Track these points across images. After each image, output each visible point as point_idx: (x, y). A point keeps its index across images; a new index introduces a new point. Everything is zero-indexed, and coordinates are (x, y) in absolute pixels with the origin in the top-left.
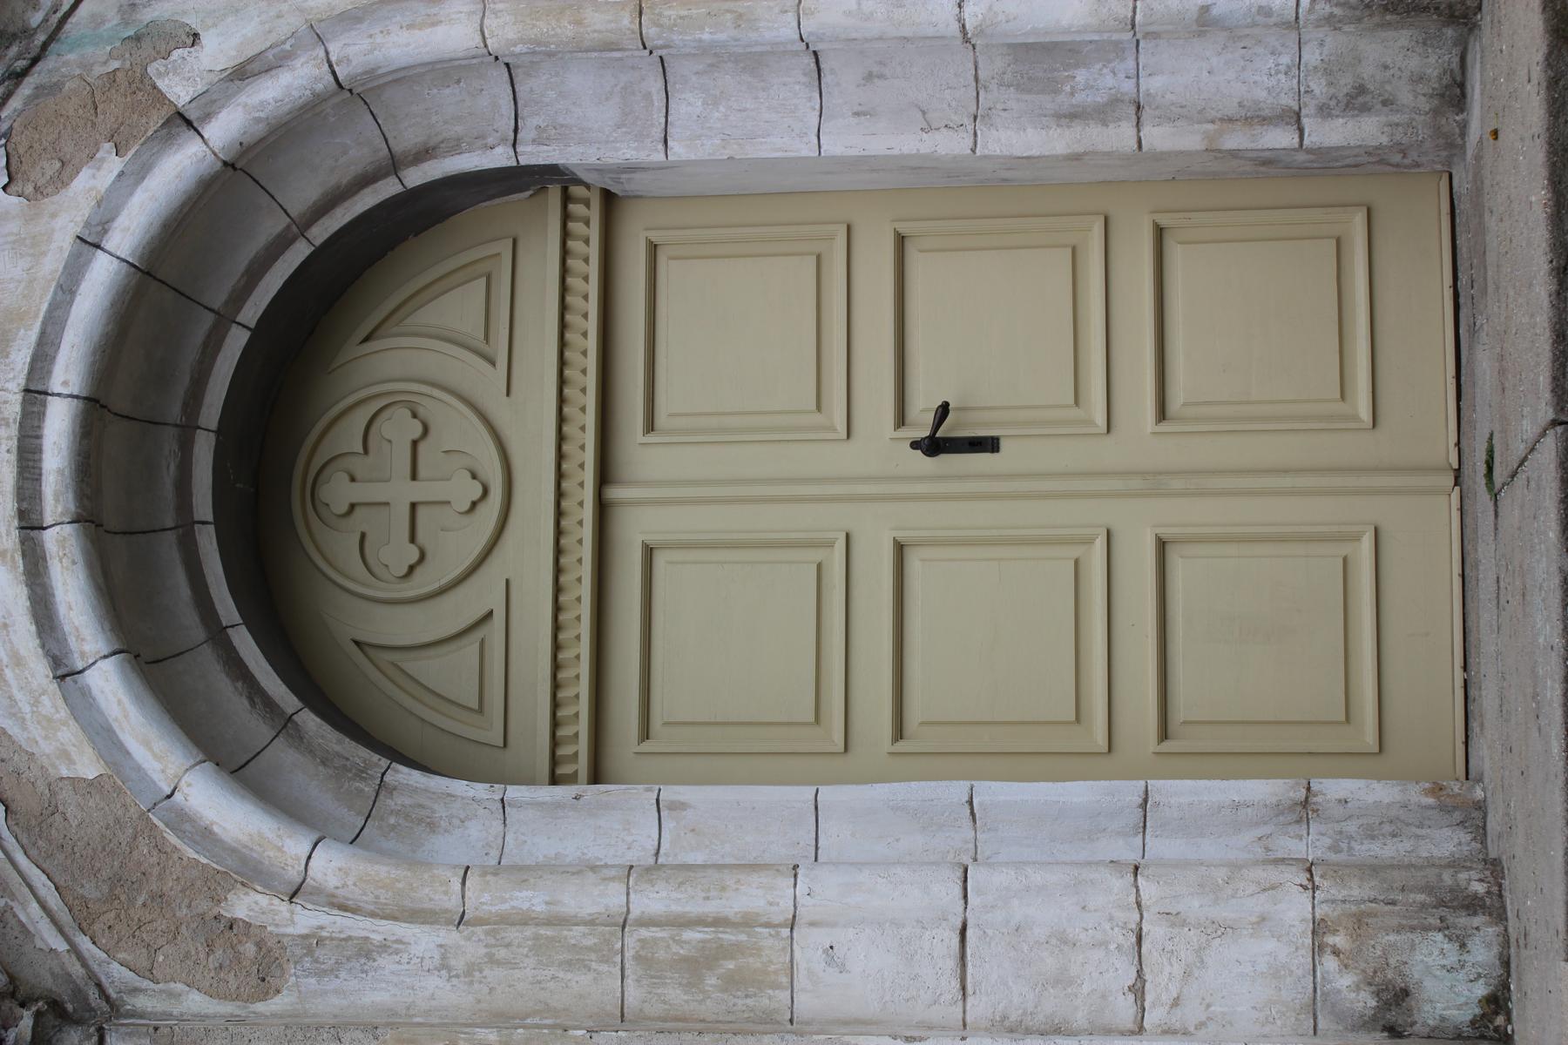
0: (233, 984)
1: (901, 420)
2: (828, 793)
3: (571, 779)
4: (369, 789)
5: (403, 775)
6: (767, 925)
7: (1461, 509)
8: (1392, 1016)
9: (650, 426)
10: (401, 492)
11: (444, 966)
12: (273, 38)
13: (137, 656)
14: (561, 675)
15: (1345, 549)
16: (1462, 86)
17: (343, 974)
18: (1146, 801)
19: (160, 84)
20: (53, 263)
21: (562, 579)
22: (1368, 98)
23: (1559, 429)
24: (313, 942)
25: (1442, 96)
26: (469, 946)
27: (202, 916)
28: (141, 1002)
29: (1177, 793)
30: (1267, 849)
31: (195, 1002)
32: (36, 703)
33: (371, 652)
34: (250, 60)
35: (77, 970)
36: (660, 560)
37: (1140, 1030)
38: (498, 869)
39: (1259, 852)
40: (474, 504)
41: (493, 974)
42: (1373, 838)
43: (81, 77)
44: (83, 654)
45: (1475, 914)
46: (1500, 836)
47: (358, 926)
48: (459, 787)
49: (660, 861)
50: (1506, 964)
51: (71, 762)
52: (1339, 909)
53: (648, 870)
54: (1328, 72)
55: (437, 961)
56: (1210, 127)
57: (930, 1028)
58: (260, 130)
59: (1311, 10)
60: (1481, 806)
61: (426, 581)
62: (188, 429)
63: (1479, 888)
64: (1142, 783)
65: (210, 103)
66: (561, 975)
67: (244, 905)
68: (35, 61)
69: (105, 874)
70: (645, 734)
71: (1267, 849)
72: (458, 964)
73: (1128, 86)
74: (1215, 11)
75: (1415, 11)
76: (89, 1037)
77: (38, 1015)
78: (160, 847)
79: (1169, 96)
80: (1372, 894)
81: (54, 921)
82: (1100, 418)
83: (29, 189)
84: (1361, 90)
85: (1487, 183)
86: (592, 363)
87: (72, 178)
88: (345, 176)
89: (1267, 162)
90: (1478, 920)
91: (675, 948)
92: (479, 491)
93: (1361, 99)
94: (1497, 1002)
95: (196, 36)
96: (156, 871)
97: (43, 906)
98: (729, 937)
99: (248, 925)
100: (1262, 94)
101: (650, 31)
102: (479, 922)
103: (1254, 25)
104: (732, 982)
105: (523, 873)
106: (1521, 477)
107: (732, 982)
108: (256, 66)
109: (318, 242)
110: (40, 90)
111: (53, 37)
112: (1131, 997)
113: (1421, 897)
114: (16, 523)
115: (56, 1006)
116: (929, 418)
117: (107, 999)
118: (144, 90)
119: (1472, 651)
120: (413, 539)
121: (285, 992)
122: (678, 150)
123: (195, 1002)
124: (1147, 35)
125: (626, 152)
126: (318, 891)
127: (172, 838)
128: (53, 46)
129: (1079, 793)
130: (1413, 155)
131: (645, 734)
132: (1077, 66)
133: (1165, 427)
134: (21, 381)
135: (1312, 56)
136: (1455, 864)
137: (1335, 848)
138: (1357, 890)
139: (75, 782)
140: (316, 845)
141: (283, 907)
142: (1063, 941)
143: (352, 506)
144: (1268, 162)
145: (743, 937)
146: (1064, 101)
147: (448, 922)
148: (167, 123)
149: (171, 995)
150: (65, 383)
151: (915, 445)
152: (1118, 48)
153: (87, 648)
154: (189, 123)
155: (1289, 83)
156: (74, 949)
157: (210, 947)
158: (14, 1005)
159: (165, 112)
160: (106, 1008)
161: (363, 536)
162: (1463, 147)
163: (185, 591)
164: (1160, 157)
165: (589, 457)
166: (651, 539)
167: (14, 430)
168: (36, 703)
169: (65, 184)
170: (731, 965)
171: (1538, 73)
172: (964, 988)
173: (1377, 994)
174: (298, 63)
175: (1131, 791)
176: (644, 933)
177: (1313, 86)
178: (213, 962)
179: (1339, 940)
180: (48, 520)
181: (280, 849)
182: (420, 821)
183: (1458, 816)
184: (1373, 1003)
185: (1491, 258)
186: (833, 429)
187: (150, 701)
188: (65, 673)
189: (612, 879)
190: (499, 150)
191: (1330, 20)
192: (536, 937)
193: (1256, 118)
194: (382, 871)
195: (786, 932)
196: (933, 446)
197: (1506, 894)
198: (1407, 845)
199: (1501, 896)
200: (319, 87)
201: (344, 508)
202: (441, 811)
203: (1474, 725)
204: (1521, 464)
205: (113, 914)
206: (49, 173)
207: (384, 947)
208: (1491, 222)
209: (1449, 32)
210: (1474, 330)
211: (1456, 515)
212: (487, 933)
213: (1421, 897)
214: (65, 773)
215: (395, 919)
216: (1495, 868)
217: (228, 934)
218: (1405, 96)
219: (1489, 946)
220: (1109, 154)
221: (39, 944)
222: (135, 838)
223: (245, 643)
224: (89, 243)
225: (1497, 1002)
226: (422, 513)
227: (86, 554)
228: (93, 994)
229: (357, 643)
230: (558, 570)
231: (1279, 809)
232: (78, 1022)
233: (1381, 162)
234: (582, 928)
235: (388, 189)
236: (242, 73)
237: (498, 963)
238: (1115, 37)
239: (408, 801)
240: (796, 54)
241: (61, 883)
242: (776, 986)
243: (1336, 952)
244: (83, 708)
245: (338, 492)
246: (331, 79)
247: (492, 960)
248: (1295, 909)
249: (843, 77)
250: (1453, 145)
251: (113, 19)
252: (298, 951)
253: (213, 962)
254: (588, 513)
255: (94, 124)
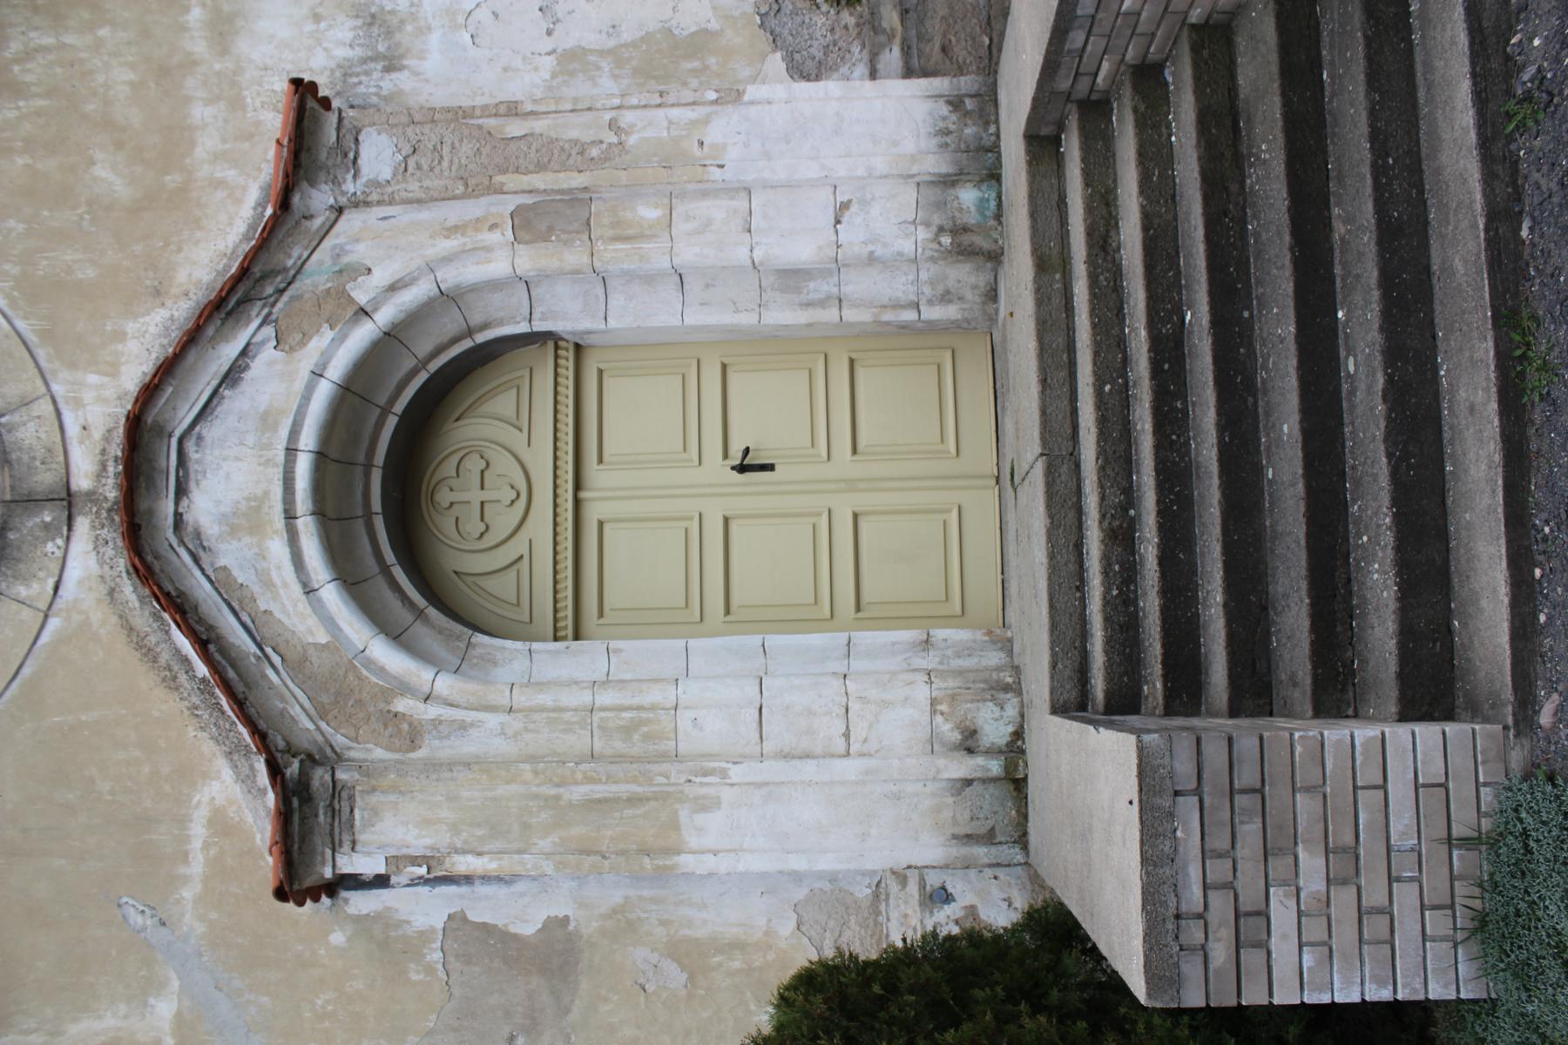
0: (398, 745)
1: (726, 456)
2: (692, 642)
3: (564, 638)
4: (463, 645)
5: (480, 638)
6: (663, 709)
7: (1000, 496)
8: (969, 743)
9: (600, 461)
10: (476, 496)
11: (503, 733)
12: (408, 271)
13: (345, 582)
14: (558, 586)
15: (945, 516)
16: (995, 290)
17: (452, 738)
18: (849, 642)
19: (353, 294)
20: (299, 385)
21: (558, 519)
22: (951, 296)
23: (1044, 458)
24: (436, 723)
25: (986, 295)
26: (515, 723)
27: (381, 711)
28: (352, 754)
29: (864, 638)
30: (909, 664)
31: (379, 753)
32: (295, 606)
33: (463, 576)
34: (397, 281)
35: (320, 738)
36: (607, 528)
37: (848, 754)
38: (529, 684)
39: (905, 666)
40: (513, 502)
41: (527, 737)
42: (959, 657)
43: (313, 292)
44: (317, 581)
45: (1007, 692)
46: (1019, 654)
47: (459, 714)
48: (508, 643)
49: (610, 678)
50: (1022, 716)
51: (313, 635)
52: (943, 692)
53: (604, 683)
54: (932, 284)
55: (499, 731)
56: (875, 310)
57: (745, 757)
58: (402, 316)
59: (923, 254)
60: (1010, 640)
61: (490, 540)
62: (368, 467)
63: (1009, 680)
64: (847, 634)
65: (377, 303)
66: (561, 736)
67: (402, 705)
68: (289, 284)
69: (332, 690)
70: (601, 615)
71: (909, 664)
72: (510, 732)
73: (835, 290)
74: (876, 254)
75: (1120, 89)
76: (327, 772)
77: (302, 762)
78: (359, 677)
79: (856, 296)
80: (959, 684)
81: (308, 714)
82: (824, 454)
83: (287, 348)
84: (948, 292)
85: (1009, 337)
86: (570, 420)
87: (308, 342)
88: (445, 339)
89: (903, 327)
90: (1009, 695)
91: (618, 722)
92: (515, 495)
93: (947, 297)
94: (1018, 734)
95: (370, 270)
96: (357, 689)
97: (302, 707)
98: (644, 715)
99: (404, 715)
100: (900, 294)
101: (597, 264)
102: (520, 711)
103: (895, 260)
104: (647, 737)
105: (541, 686)
106: (1027, 481)
107: (647, 737)
108: (400, 285)
109: (432, 372)
110: (292, 299)
111: (298, 272)
112: (843, 739)
113: (982, 685)
114: (283, 516)
115: (310, 757)
116: (740, 455)
117: (335, 752)
118: (344, 297)
119: (1005, 565)
120: (482, 519)
121: (424, 747)
122: (612, 323)
123: (379, 753)
124: (843, 265)
125: (585, 324)
126: (438, 697)
127: (365, 672)
128: (299, 277)
129: (817, 639)
130: (973, 324)
131: (601, 615)
132: (809, 281)
133: (856, 457)
134: (284, 444)
135: (924, 276)
136: (999, 669)
137: (941, 663)
138: (952, 683)
139: (315, 645)
140: (437, 674)
141: (421, 706)
142: (810, 713)
143: (452, 504)
144: (904, 327)
145: (651, 715)
146: (804, 298)
147: (505, 711)
148: (356, 313)
149: (368, 750)
150: (306, 445)
151: (733, 468)
152: (830, 272)
153: (320, 578)
154: (366, 313)
155: (912, 289)
156: (318, 728)
157: (386, 726)
158: (289, 756)
159: (355, 308)
160: (335, 757)
161: (457, 519)
162: (997, 320)
163: (368, 548)
164: (851, 325)
165: (570, 477)
166: (602, 517)
167: (281, 469)
168: (295, 606)
169: (305, 345)
170: (646, 729)
171: (1030, 285)
172: (761, 737)
173: (962, 733)
174: (421, 282)
175: (842, 638)
176: (603, 714)
177: (925, 290)
178: (387, 733)
179: (943, 707)
180: (299, 513)
181: (419, 676)
182: (489, 661)
183: (999, 645)
184: (960, 737)
185: (1011, 375)
186: (692, 461)
187: (352, 603)
188: (309, 591)
189: (585, 688)
190: (522, 324)
191: (932, 259)
192: (549, 718)
193: (897, 306)
194: (471, 687)
195: (673, 712)
196: (742, 468)
197: (1023, 683)
198: (976, 660)
199: (1019, 683)
200: (432, 294)
201: (448, 505)
202: (499, 656)
203: (1007, 601)
204: (1027, 474)
205: (336, 711)
206: (297, 339)
207: (472, 725)
208: (1011, 357)
209: (989, 265)
210: (1004, 408)
211: (997, 499)
212: (524, 716)
213: (982, 685)
214: (311, 640)
215: (477, 710)
216: (1017, 670)
217: (394, 719)
218: (969, 295)
219: (1014, 708)
220: (826, 324)
221: (301, 726)
222: (346, 672)
223: (399, 574)
224: (318, 374)
225: (1018, 734)
226: (487, 506)
227: (318, 530)
228: (328, 751)
229: (455, 572)
230: (555, 534)
231: (914, 645)
232: (321, 764)
233: (959, 327)
234: (571, 713)
235: (467, 344)
236: (393, 288)
237: (530, 731)
238: (828, 266)
239: (482, 651)
240: (671, 274)
241: (311, 696)
242: (668, 739)
243: (942, 714)
244: (318, 607)
245: (444, 497)
246: (437, 290)
247: (526, 729)
248: (922, 693)
249: (693, 285)
250: (992, 319)
251: (328, 262)
252: (430, 727)
253: (387, 733)
254: (570, 505)
255: (319, 315)
